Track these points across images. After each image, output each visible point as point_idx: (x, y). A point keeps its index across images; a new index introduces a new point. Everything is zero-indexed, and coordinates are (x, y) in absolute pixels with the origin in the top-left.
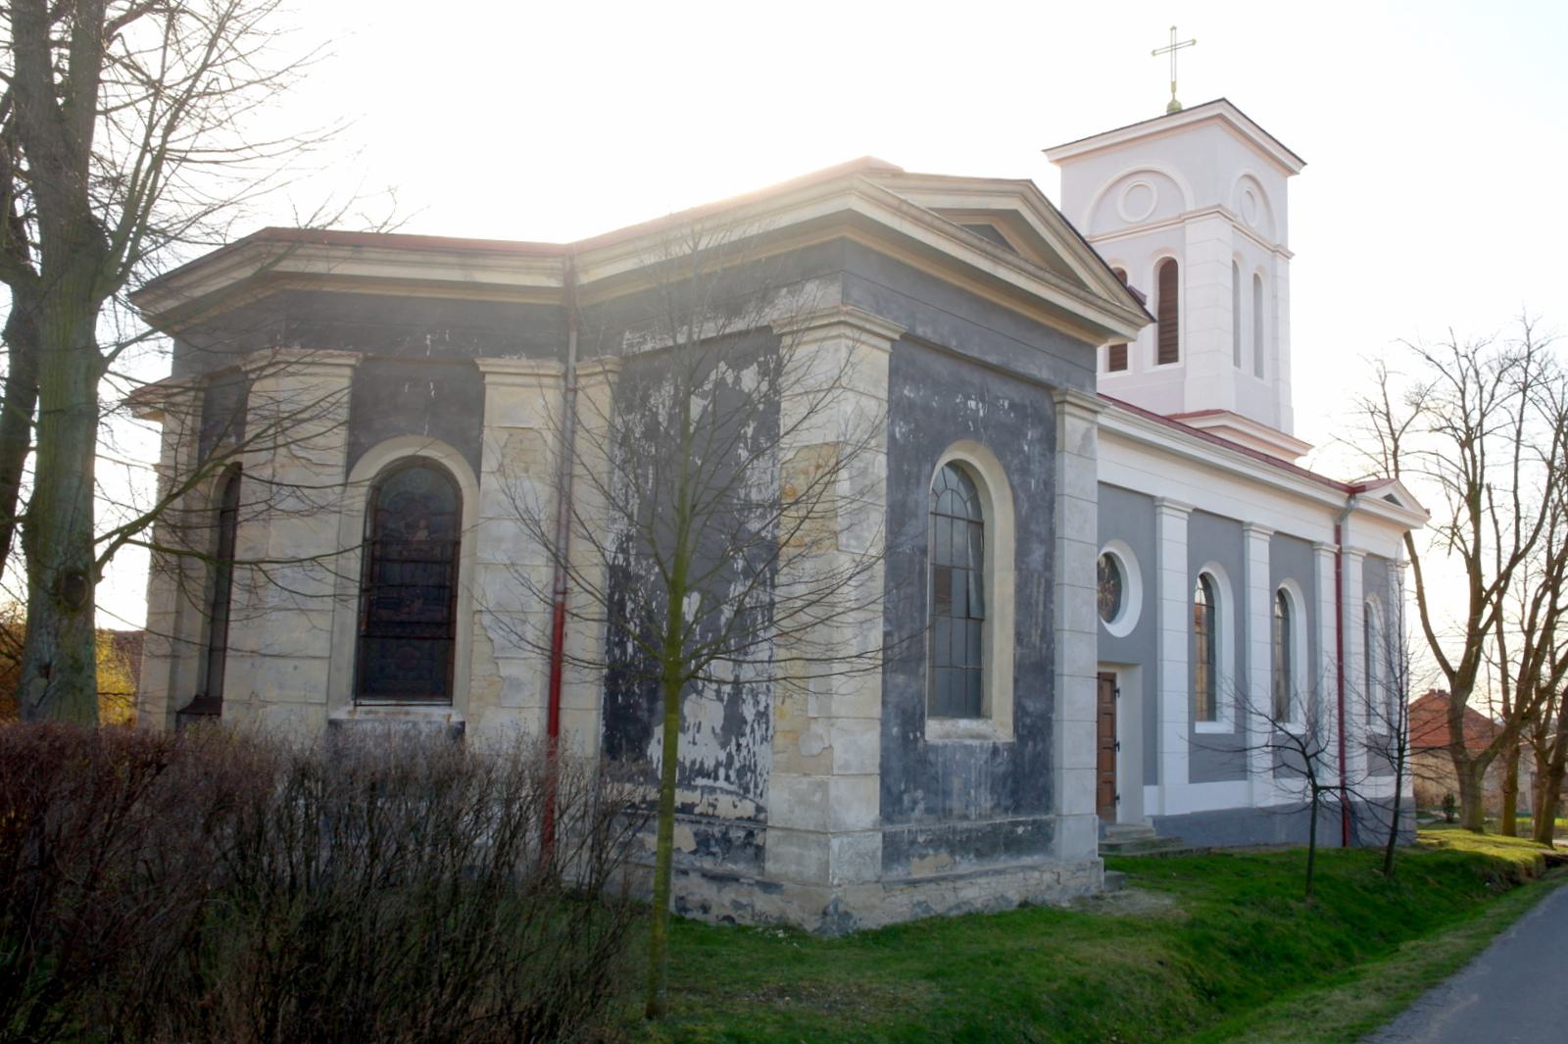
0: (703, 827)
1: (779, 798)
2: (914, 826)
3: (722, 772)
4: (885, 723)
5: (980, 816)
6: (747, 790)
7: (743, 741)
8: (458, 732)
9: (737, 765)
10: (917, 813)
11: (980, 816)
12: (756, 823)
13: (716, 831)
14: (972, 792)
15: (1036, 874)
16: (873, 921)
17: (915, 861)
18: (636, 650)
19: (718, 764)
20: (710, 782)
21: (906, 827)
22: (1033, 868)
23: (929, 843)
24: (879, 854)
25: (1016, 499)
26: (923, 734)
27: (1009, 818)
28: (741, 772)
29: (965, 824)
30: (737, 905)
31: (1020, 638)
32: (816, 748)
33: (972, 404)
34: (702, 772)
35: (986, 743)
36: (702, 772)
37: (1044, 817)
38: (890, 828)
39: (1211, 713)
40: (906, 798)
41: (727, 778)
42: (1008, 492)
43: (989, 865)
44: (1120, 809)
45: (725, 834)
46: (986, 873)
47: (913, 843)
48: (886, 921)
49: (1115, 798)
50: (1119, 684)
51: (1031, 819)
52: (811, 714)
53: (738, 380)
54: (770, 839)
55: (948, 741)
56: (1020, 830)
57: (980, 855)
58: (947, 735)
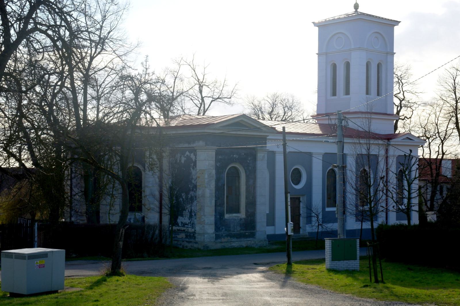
0: (186, 234)
1: (198, 228)
2: (222, 233)
3: (189, 224)
4: (215, 216)
5: (237, 231)
6: (193, 227)
7: (192, 219)
8: (143, 218)
9: (192, 223)
10: (223, 231)
11: (237, 231)
12: (194, 233)
13: (189, 234)
14: (236, 227)
15: (250, 242)
16: (212, 248)
17: (223, 239)
18: (175, 202)
19: (189, 223)
20: (187, 226)
21: (220, 233)
22: (249, 241)
23: (225, 236)
24: (215, 237)
25: (246, 172)
26: (224, 217)
27: (245, 231)
28: (192, 224)
29: (234, 233)
30: (192, 246)
31: (247, 198)
32: (202, 220)
33: (235, 156)
34: (186, 224)
35: (238, 218)
36: (186, 224)
37: (253, 231)
38: (217, 233)
39: (334, 204)
40: (221, 228)
41: (190, 225)
42: (244, 171)
43: (239, 240)
44: (301, 230)
45: (190, 235)
46: (238, 241)
47: (222, 236)
48: (216, 248)
49: (300, 228)
50: (301, 199)
51: (249, 232)
52: (202, 215)
53: (190, 155)
54: (196, 235)
55: (230, 218)
56: (247, 234)
57: (237, 238)
58: (230, 217)
